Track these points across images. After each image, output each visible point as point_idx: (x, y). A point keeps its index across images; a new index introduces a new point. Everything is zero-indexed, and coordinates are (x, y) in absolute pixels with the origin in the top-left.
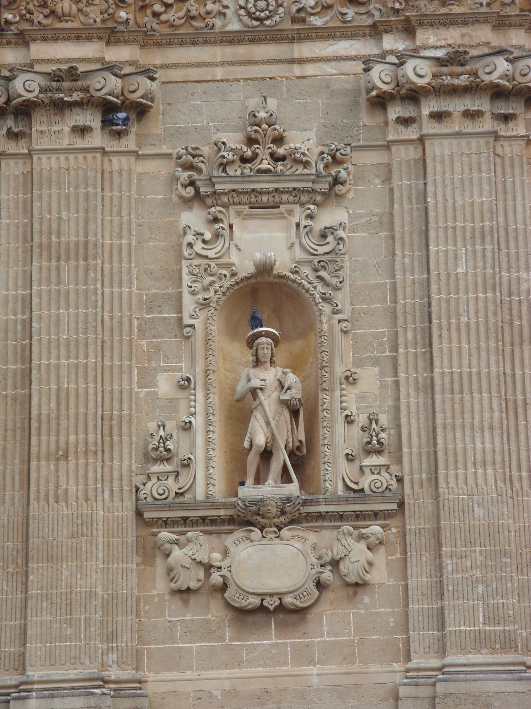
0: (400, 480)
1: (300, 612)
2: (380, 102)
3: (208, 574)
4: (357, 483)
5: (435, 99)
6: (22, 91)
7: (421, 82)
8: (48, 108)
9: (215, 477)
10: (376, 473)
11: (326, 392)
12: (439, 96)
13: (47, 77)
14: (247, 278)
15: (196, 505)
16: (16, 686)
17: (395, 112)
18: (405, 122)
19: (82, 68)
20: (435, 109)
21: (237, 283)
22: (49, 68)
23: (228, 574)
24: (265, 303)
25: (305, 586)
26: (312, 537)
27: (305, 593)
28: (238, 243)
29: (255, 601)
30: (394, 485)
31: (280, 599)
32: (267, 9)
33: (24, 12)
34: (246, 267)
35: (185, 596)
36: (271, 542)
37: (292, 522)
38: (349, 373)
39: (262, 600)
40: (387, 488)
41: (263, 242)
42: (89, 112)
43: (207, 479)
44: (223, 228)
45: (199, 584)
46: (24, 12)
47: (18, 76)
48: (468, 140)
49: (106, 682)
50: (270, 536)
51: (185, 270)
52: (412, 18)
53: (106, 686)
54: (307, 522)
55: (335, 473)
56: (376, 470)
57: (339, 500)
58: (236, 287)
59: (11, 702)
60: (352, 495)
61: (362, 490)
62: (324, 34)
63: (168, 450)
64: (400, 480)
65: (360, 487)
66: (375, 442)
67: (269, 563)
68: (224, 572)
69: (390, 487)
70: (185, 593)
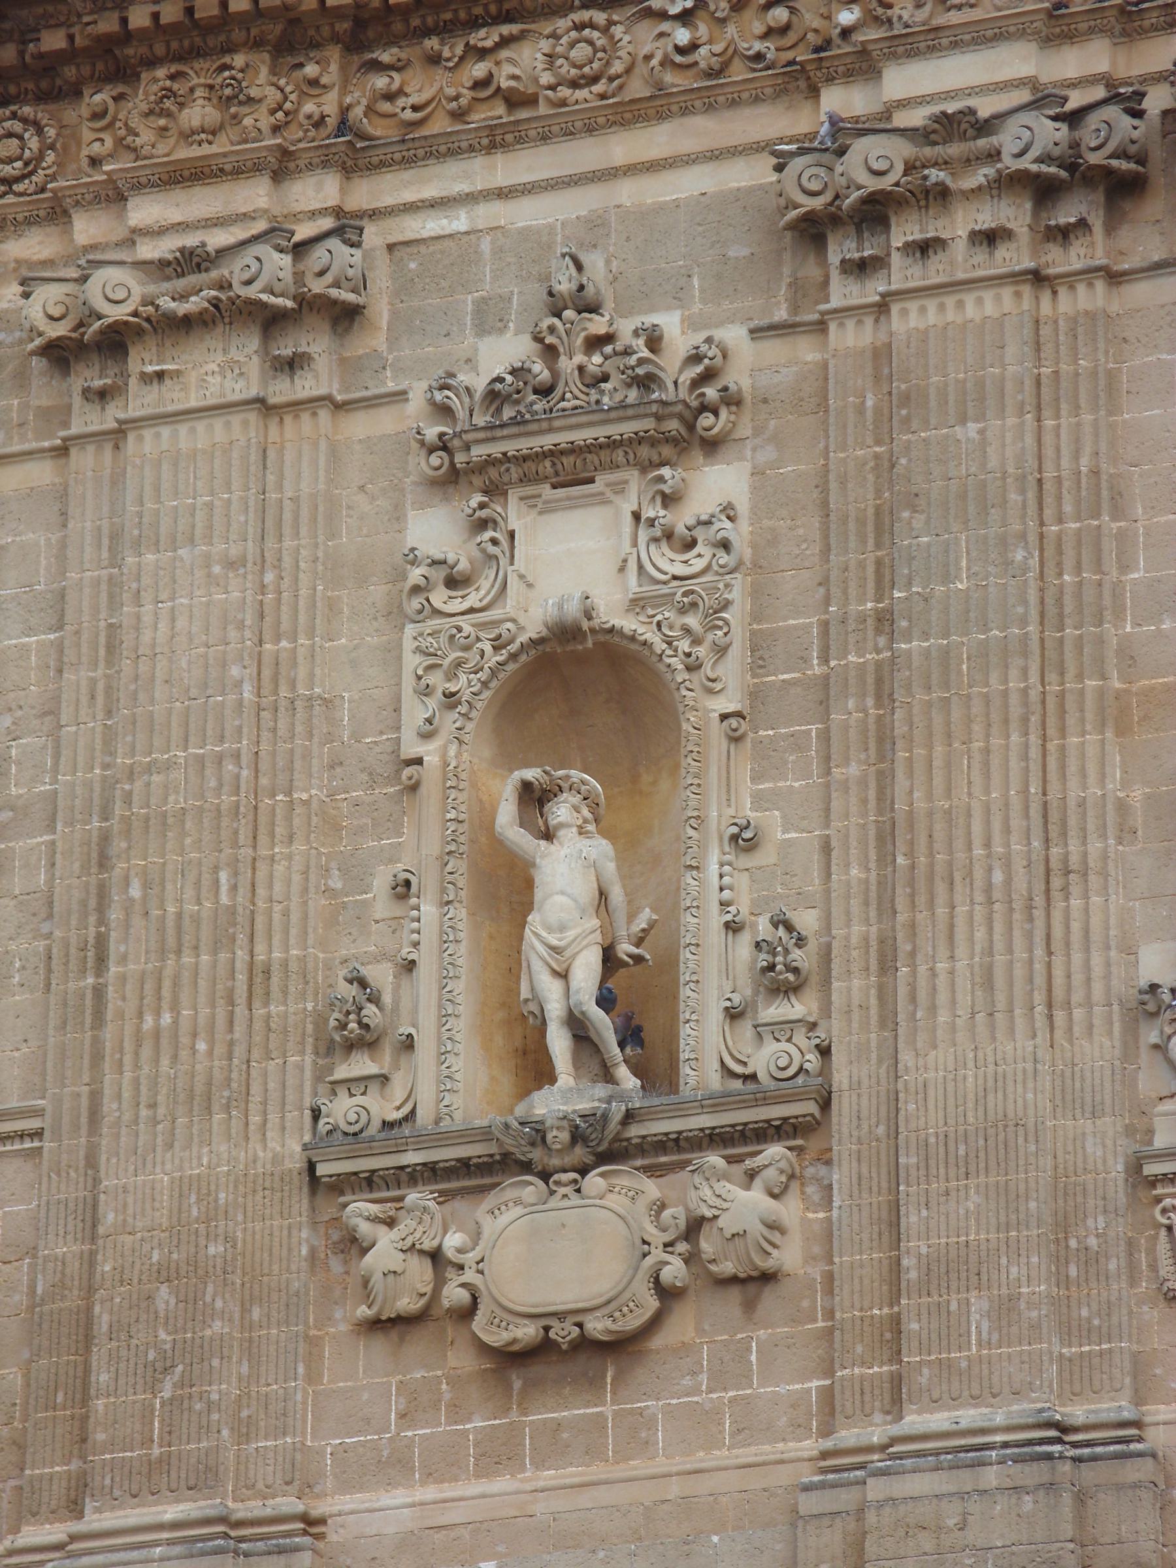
0: (825, 1051)
1: (622, 1348)
2: (812, 231)
3: (440, 1282)
4: (745, 1064)
5: (915, 216)
6: (863, 177)
7: (886, 183)
8: (923, 203)
9: (457, 1076)
10: (783, 1039)
11: (694, 873)
12: (927, 207)
13: (912, 140)
14: (534, 643)
15: (424, 1140)
16: (883, 1448)
17: (842, 247)
18: (861, 268)
19: (986, 107)
20: (918, 236)
21: (513, 657)
22: (916, 118)
23: (476, 1280)
24: (581, 693)
25: (627, 1295)
26: (651, 1188)
27: (631, 1304)
28: (523, 571)
29: (527, 1332)
30: (813, 1061)
31: (580, 1325)
32: (20, 158)
33: (123, 132)
34: (533, 624)
35: (752, 1288)
36: (566, 1203)
37: (605, 1158)
38: (735, 830)
39: (547, 1329)
40: (801, 1069)
41: (574, 560)
42: (1003, 203)
43: (450, 1082)
44: (494, 542)
45: (422, 1302)
46: (123, 132)
47: (848, 147)
48: (957, 297)
49: (1064, 1429)
50: (563, 1190)
51: (408, 644)
52: (870, 47)
53: (1067, 1438)
54: (643, 1157)
55: (705, 1045)
56: (784, 1029)
57: (717, 1102)
58: (511, 667)
59: (869, 1481)
60: (737, 1084)
61: (753, 1077)
62: (649, 111)
63: (796, 971)
64: (825, 1051)
65: (748, 1071)
66: (353, 1025)
67: (555, 1253)
68: (469, 1276)
69: (807, 1066)
70: (385, 1325)
